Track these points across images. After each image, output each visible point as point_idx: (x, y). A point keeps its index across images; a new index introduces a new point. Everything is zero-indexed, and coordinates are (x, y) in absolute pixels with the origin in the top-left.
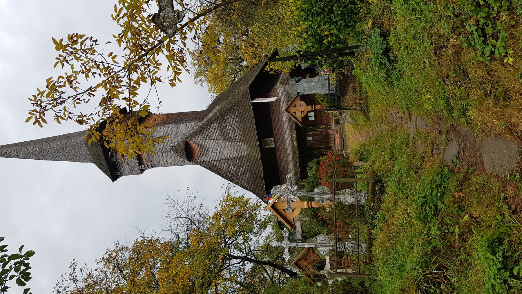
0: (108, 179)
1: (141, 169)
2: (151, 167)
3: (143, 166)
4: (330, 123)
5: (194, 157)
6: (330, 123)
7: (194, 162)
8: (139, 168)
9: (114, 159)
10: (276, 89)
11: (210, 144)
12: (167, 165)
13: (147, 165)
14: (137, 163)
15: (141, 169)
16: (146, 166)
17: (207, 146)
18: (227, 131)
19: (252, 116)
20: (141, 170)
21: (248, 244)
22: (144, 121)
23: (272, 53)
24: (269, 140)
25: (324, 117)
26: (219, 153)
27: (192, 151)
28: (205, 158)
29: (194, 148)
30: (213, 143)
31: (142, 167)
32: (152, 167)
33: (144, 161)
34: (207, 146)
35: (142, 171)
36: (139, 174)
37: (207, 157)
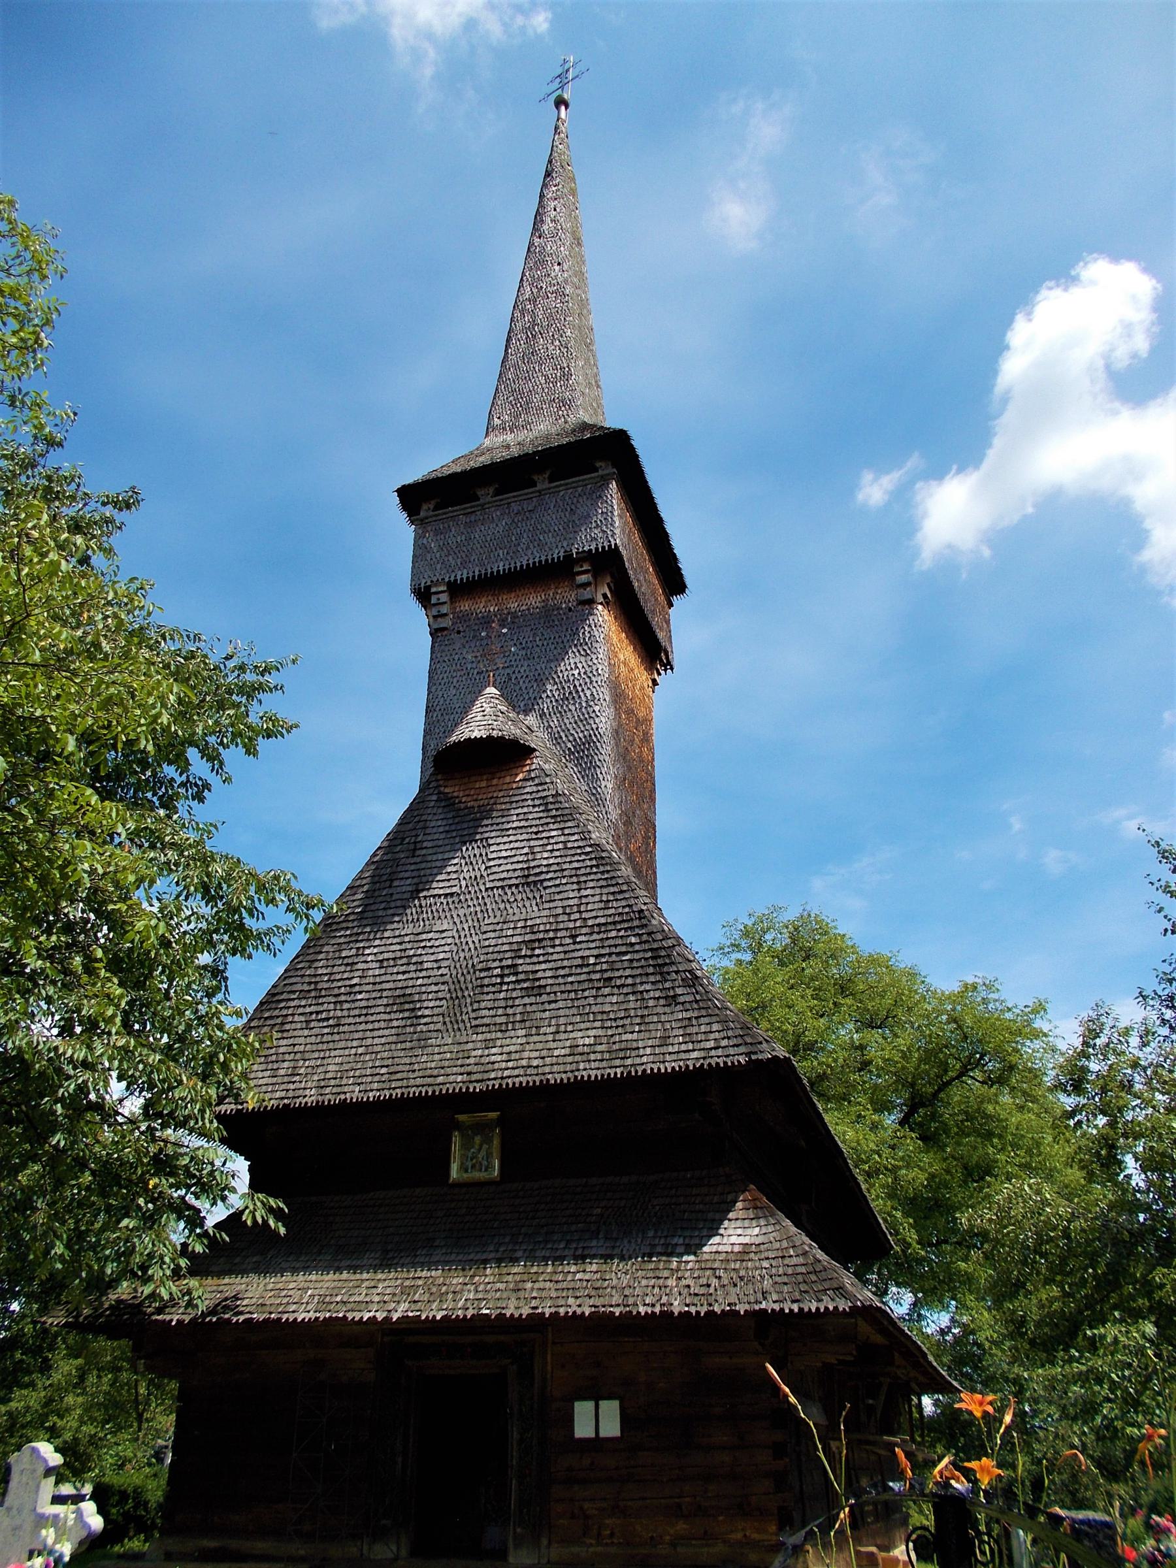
0: (409, 480)
1: (433, 590)
2: (436, 626)
3: (444, 597)
4: (545, 1542)
5: (450, 783)
6: (545, 1542)
7: (429, 782)
8: (437, 583)
9: (489, 499)
10: (773, 1215)
11: (504, 854)
12: (433, 690)
13: (446, 615)
14: (462, 575)
15: (433, 590)
16: (444, 609)
17: (499, 840)
18: (523, 1230)
19: (629, 1062)
20: (428, 588)
21: (123, 1115)
22: (630, 628)
23: (717, 1308)
24: (489, 1155)
25: (586, 1505)
26: (454, 890)
27: (481, 774)
28: (441, 829)
29: (495, 782)
30: (509, 867)
31: (440, 596)
32: (437, 630)
33: (465, 606)
34: (499, 840)
35: (423, 595)
36: (412, 580)
37: (442, 836)
